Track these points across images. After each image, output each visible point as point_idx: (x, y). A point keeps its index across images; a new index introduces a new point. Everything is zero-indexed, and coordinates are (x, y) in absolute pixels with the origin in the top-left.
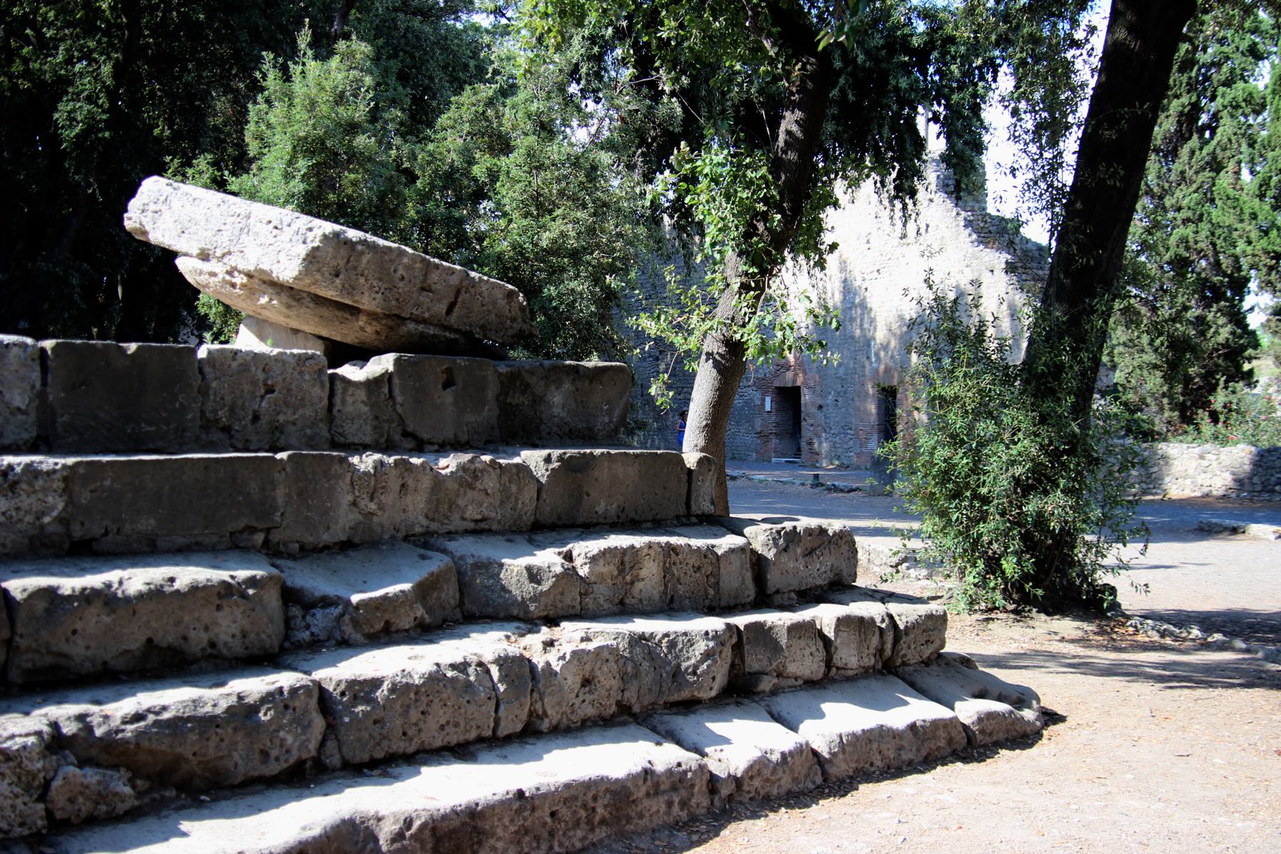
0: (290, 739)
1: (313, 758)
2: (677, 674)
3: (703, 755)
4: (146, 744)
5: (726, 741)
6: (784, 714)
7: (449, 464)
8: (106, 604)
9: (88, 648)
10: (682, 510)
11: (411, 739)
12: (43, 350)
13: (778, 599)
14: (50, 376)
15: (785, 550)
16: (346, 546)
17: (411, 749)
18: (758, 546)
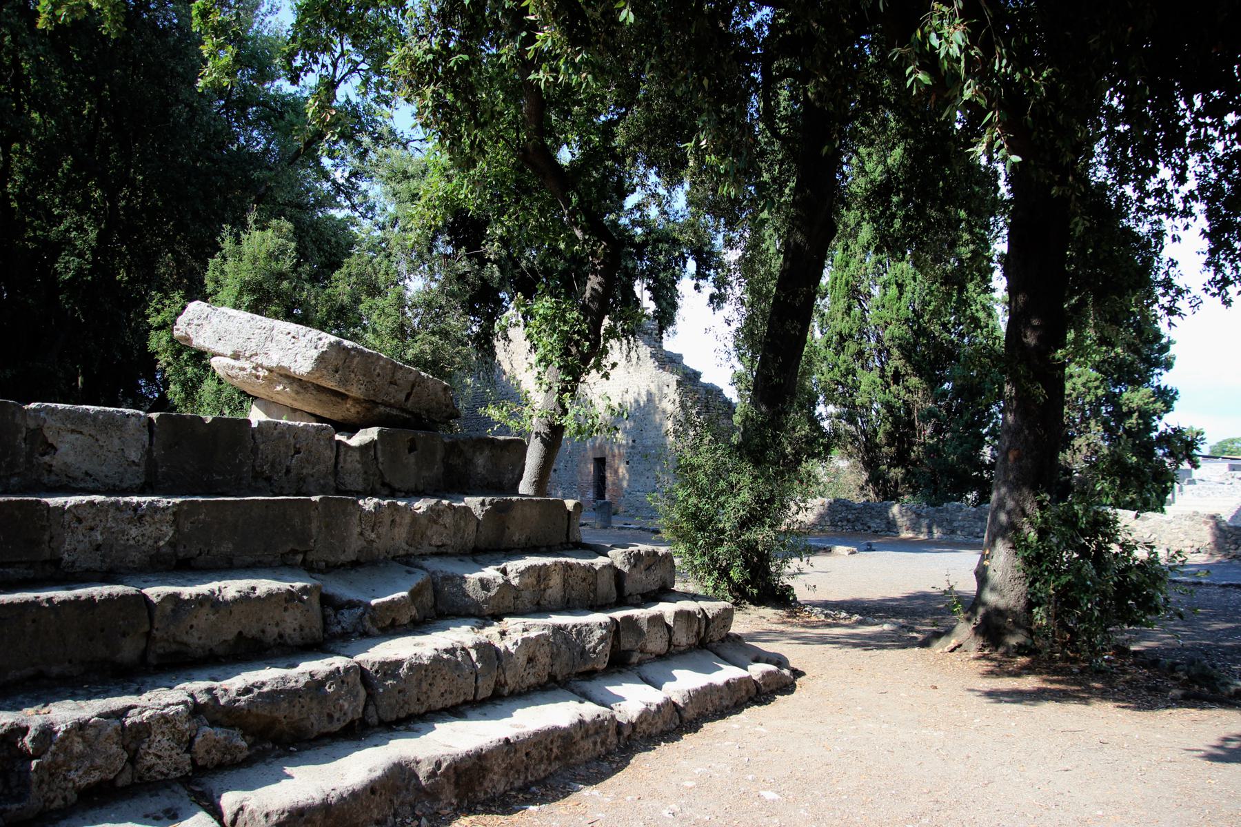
0: (346, 705)
1: (360, 719)
2: (583, 653)
3: (612, 709)
4: (254, 710)
5: (622, 699)
6: (650, 678)
7: (421, 505)
8: (212, 606)
9: (200, 638)
10: (564, 540)
11: (423, 704)
12: (150, 419)
13: (630, 600)
14: (155, 439)
15: (635, 566)
16: (356, 564)
17: (423, 711)
18: (618, 565)
